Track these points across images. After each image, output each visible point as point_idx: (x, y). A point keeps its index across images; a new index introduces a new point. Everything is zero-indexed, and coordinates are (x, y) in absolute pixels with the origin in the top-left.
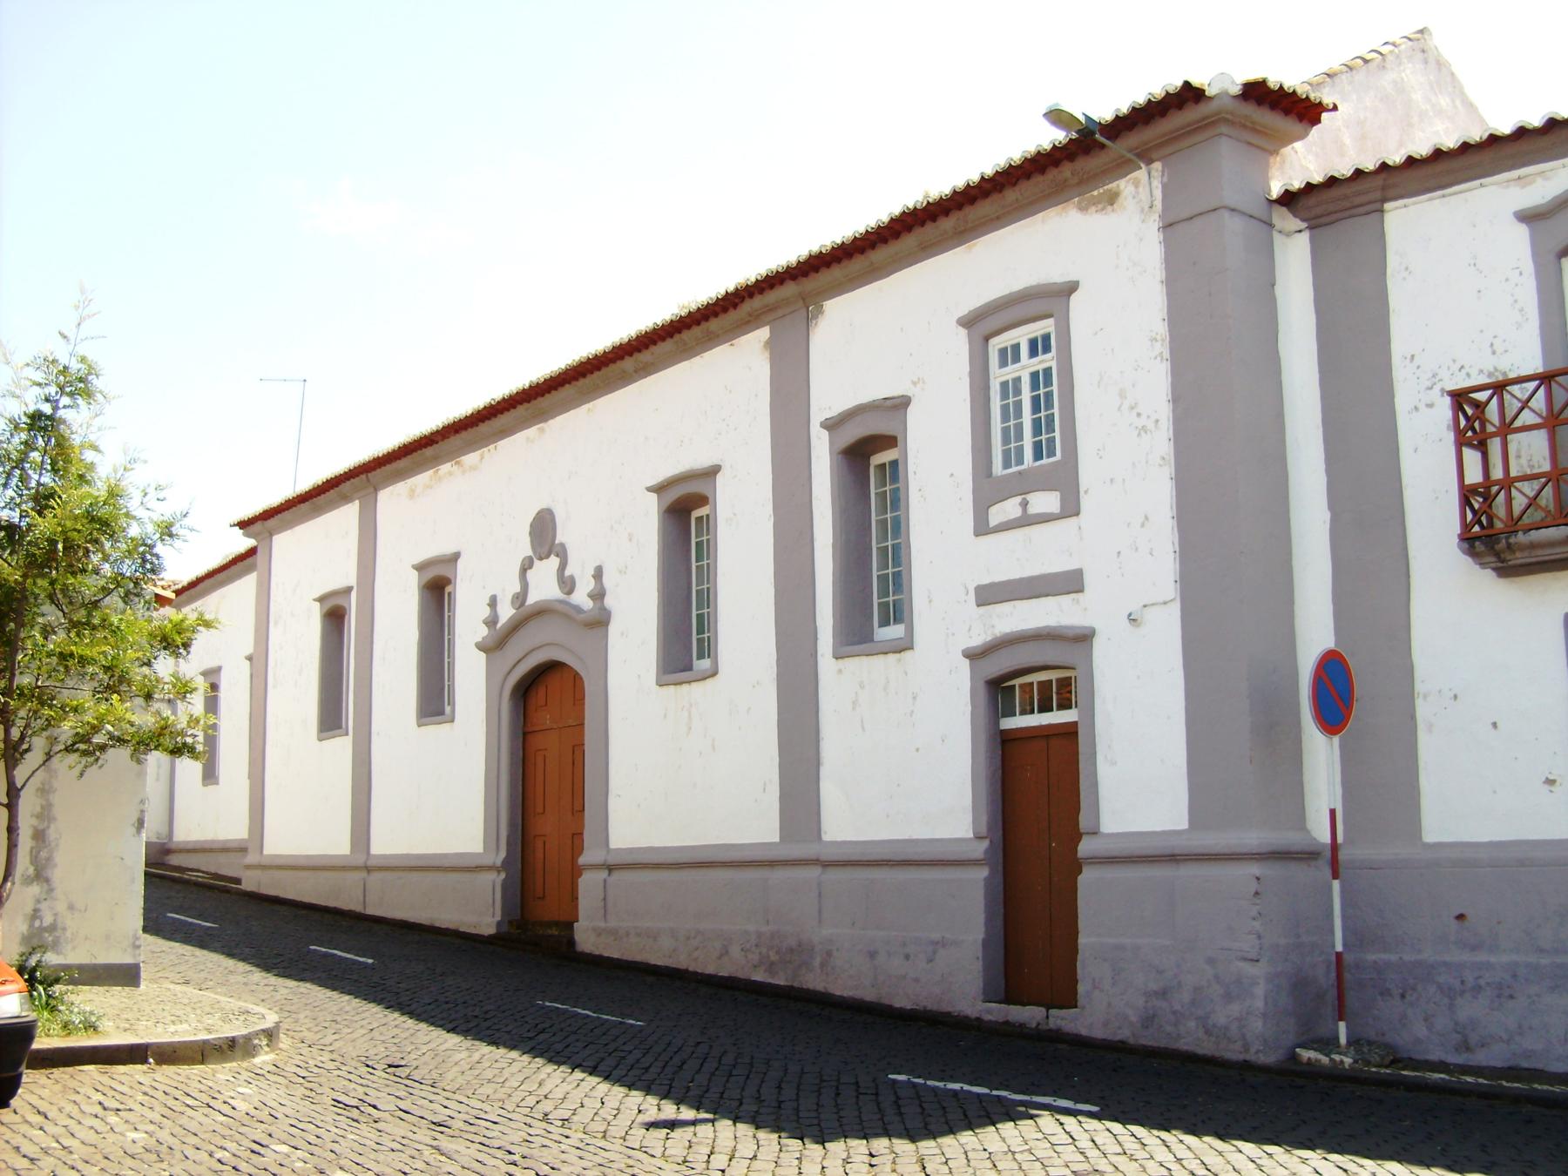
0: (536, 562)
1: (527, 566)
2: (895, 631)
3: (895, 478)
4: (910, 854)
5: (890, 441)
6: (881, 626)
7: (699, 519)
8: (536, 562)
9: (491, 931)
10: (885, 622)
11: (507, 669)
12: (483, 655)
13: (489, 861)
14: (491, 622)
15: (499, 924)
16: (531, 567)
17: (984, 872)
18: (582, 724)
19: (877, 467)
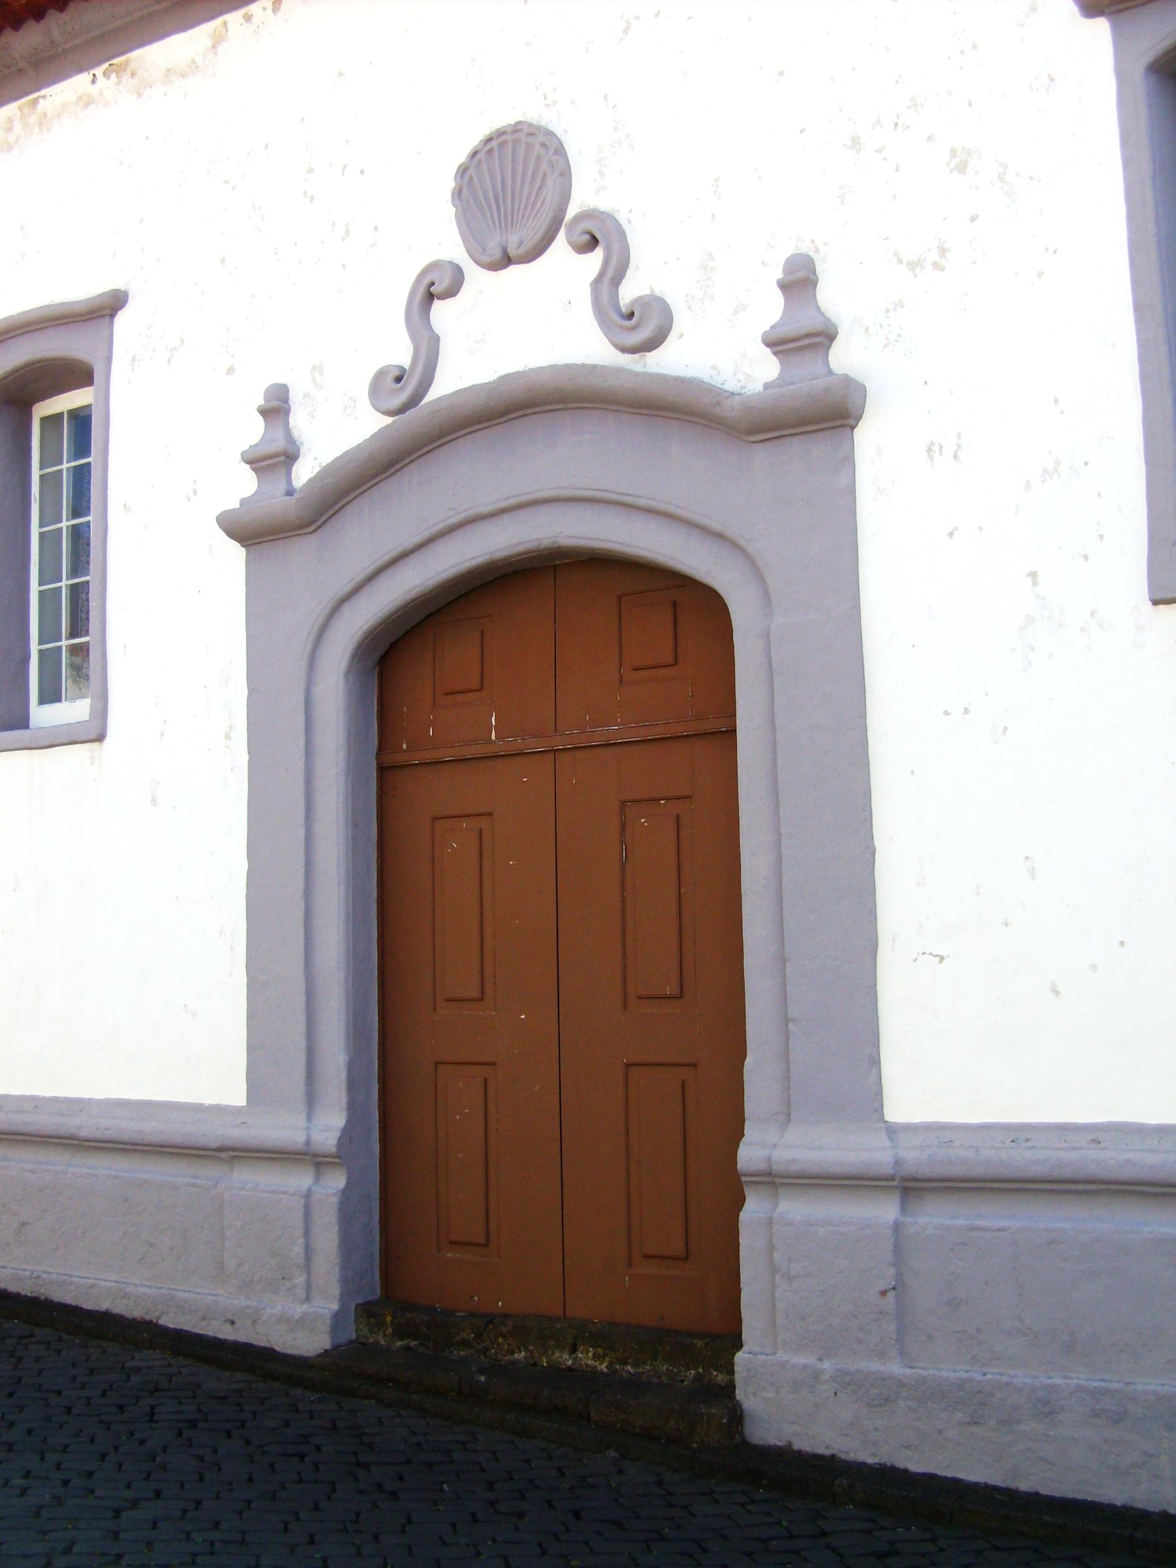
0: (477, 278)
1: (434, 289)
2: (73, 711)
3: (82, 445)
4: (87, 1126)
5: (77, 374)
6: (42, 701)
7: (52, 422)
8: (477, 278)
9: (310, 1342)
10: (51, 695)
11: (343, 585)
12: (236, 553)
13: (286, 1128)
14: (273, 460)
15: (337, 1319)
16: (452, 291)
17: (336, 1181)
18: (732, 732)
19: (44, 420)
